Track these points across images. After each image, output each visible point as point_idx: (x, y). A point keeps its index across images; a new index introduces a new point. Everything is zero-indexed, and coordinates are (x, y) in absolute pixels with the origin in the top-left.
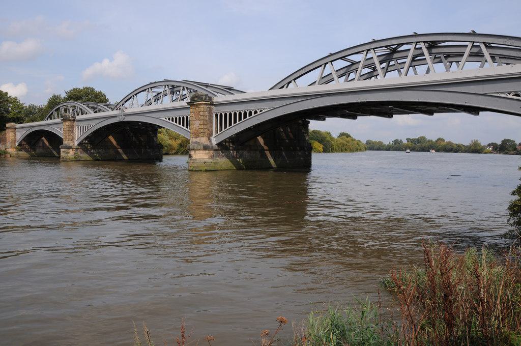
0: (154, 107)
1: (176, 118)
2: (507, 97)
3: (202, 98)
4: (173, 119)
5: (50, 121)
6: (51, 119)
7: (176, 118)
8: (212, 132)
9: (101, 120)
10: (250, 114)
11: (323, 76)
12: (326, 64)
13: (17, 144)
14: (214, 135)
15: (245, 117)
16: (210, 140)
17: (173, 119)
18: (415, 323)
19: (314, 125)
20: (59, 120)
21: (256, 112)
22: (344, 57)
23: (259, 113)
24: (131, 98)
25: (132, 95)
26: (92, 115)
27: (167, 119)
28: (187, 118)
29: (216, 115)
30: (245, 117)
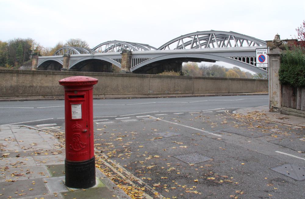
0: (107, 53)
1: (116, 59)
2: (147, 52)
3: (126, 52)
4: (115, 59)
5: (56, 56)
6: (57, 55)
7: (116, 59)
8: (131, 66)
9: (82, 58)
10: (146, 59)
11: (179, 45)
12: (180, 40)
13: (37, 67)
14: (132, 68)
15: (144, 61)
16: (129, 70)
17: (115, 59)
18: (129, 177)
19: (184, 64)
20: (62, 56)
21: (148, 59)
22: (190, 37)
23: (149, 59)
24: (98, 47)
25: (99, 46)
26: (79, 54)
27: (238, 59)
28: (121, 59)
29: (133, 59)
30: (144, 61)
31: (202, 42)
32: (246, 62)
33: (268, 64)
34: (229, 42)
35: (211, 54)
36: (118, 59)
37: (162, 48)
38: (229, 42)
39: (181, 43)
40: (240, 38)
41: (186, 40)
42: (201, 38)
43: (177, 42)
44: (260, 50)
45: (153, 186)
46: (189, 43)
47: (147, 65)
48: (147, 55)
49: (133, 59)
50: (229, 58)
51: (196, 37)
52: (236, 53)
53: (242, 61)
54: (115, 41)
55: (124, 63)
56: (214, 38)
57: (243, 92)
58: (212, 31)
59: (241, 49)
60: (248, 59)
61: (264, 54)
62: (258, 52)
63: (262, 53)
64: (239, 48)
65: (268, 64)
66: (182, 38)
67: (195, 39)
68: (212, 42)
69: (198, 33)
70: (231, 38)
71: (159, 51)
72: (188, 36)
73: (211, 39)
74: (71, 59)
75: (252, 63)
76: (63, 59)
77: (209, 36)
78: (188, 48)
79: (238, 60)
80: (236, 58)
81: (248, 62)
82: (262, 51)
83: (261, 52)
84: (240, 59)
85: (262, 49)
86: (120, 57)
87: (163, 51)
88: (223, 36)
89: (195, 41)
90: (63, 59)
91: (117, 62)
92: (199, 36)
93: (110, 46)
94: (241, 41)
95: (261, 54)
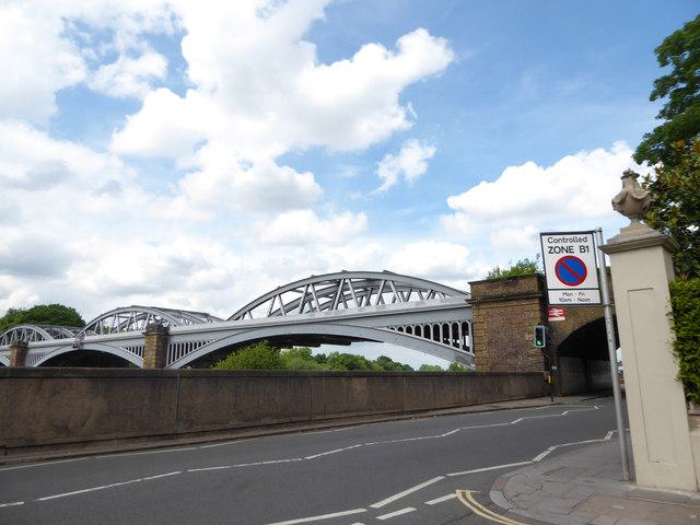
11: (273, 310)
26: (52, 341)
31: (323, 300)
32: (422, 337)
33: (600, 289)
34: (380, 298)
35: (345, 323)
37: (237, 317)
38: (380, 298)
39: (277, 305)
40: (408, 285)
41: (289, 297)
42: (311, 327)
43: (269, 303)
44: (561, 237)
46: (295, 304)
50: (385, 329)
51: (310, 290)
53: (413, 335)
54: (133, 307)
55: (152, 355)
56: (348, 289)
57: (428, 410)
58: (344, 272)
61: (577, 254)
62: (554, 245)
63: (569, 249)
64: (401, 306)
65: (600, 289)
66: (279, 292)
67: (307, 294)
68: (344, 299)
69: (314, 281)
70: (387, 289)
71: (233, 324)
72: (293, 288)
73: (342, 293)
74: (32, 352)
76: (9, 353)
77: (337, 285)
78: (294, 315)
80: (401, 329)
81: (427, 335)
82: (569, 244)
83: (565, 245)
84: (409, 330)
85: (578, 236)
87: (240, 323)
88: (370, 284)
89: (308, 298)
90: (9, 353)
92: (317, 288)
93: (122, 320)
94: (405, 294)
95: (565, 254)
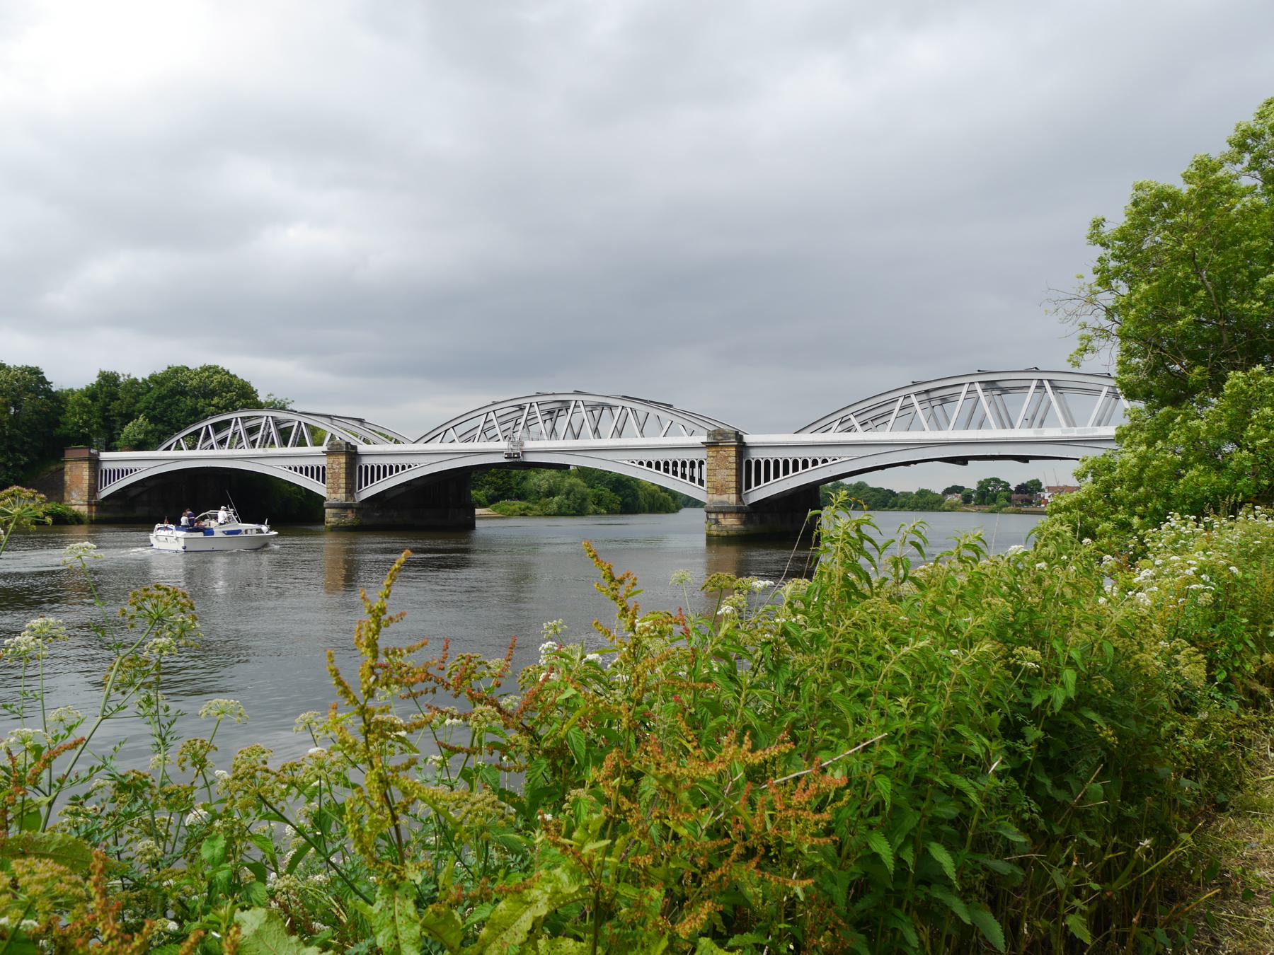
1: (307, 468)
4: (301, 468)
7: (307, 468)
10: (403, 468)
17: (301, 468)
23: (413, 467)
25: (390, 435)
27: (645, 464)
28: (324, 468)
36: (312, 468)
45: (1133, 514)
47: (134, 492)
48: (390, 458)
49: (361, 467)
52: (288, 459)
59: (1095, 434)
60: (666, 463)
75: (692, 479)
79: (645, 467)
80: (641, 463)
86: (323, 462)
91: (315, 480)
